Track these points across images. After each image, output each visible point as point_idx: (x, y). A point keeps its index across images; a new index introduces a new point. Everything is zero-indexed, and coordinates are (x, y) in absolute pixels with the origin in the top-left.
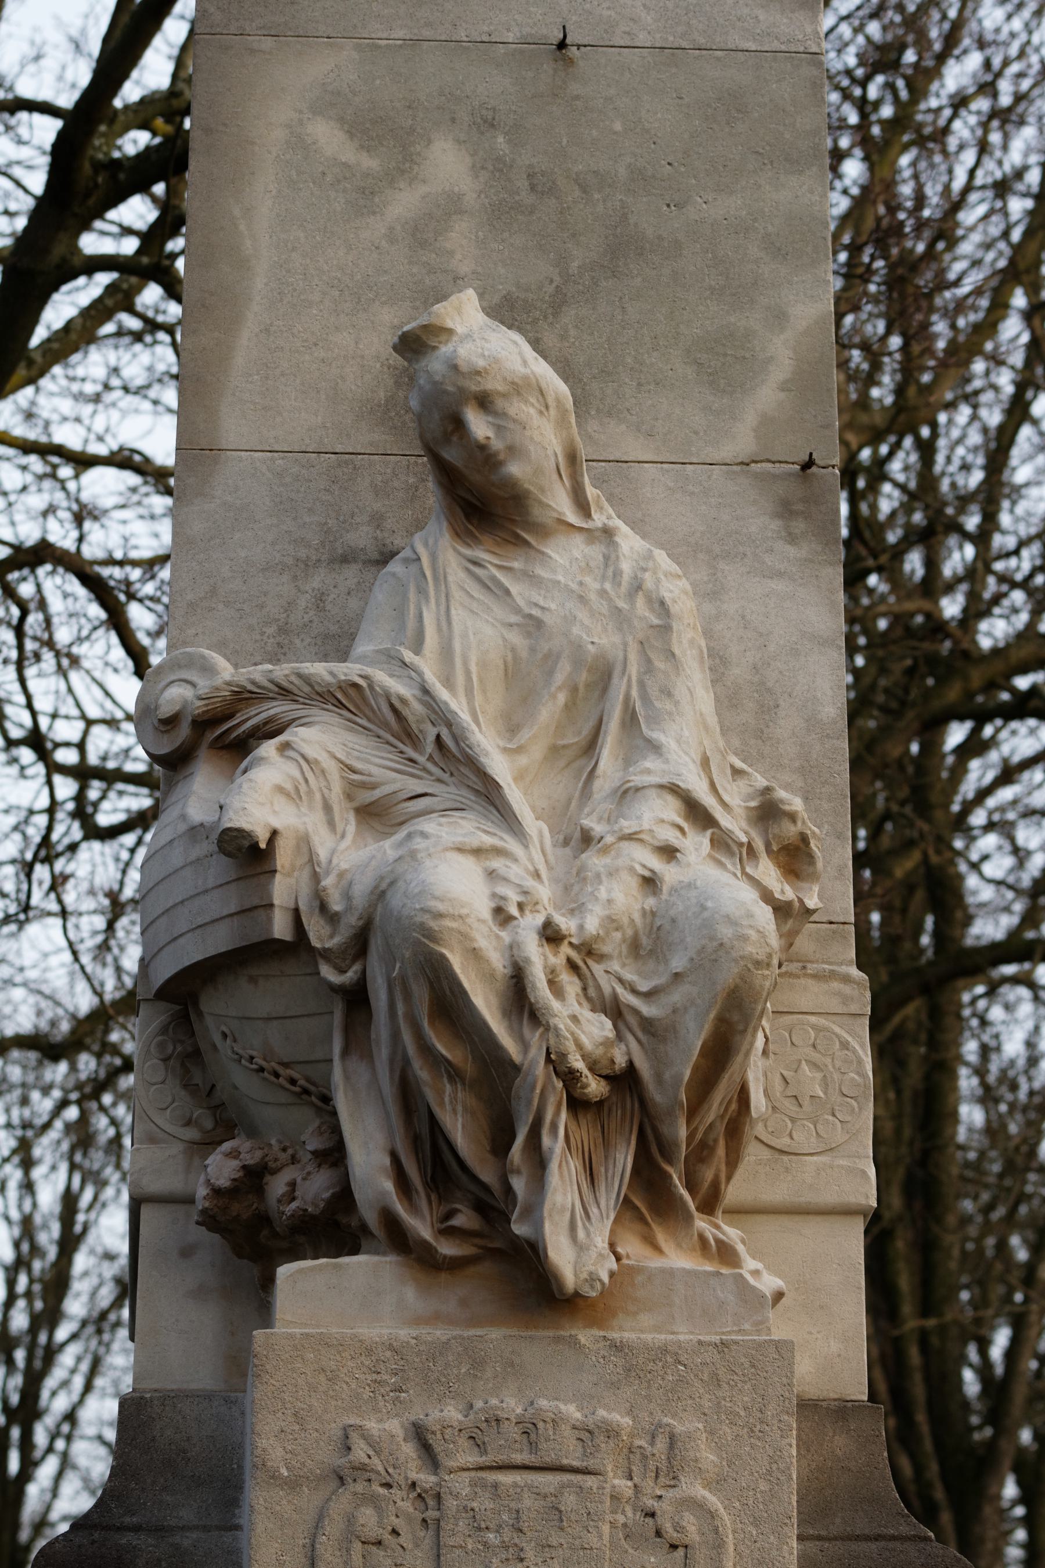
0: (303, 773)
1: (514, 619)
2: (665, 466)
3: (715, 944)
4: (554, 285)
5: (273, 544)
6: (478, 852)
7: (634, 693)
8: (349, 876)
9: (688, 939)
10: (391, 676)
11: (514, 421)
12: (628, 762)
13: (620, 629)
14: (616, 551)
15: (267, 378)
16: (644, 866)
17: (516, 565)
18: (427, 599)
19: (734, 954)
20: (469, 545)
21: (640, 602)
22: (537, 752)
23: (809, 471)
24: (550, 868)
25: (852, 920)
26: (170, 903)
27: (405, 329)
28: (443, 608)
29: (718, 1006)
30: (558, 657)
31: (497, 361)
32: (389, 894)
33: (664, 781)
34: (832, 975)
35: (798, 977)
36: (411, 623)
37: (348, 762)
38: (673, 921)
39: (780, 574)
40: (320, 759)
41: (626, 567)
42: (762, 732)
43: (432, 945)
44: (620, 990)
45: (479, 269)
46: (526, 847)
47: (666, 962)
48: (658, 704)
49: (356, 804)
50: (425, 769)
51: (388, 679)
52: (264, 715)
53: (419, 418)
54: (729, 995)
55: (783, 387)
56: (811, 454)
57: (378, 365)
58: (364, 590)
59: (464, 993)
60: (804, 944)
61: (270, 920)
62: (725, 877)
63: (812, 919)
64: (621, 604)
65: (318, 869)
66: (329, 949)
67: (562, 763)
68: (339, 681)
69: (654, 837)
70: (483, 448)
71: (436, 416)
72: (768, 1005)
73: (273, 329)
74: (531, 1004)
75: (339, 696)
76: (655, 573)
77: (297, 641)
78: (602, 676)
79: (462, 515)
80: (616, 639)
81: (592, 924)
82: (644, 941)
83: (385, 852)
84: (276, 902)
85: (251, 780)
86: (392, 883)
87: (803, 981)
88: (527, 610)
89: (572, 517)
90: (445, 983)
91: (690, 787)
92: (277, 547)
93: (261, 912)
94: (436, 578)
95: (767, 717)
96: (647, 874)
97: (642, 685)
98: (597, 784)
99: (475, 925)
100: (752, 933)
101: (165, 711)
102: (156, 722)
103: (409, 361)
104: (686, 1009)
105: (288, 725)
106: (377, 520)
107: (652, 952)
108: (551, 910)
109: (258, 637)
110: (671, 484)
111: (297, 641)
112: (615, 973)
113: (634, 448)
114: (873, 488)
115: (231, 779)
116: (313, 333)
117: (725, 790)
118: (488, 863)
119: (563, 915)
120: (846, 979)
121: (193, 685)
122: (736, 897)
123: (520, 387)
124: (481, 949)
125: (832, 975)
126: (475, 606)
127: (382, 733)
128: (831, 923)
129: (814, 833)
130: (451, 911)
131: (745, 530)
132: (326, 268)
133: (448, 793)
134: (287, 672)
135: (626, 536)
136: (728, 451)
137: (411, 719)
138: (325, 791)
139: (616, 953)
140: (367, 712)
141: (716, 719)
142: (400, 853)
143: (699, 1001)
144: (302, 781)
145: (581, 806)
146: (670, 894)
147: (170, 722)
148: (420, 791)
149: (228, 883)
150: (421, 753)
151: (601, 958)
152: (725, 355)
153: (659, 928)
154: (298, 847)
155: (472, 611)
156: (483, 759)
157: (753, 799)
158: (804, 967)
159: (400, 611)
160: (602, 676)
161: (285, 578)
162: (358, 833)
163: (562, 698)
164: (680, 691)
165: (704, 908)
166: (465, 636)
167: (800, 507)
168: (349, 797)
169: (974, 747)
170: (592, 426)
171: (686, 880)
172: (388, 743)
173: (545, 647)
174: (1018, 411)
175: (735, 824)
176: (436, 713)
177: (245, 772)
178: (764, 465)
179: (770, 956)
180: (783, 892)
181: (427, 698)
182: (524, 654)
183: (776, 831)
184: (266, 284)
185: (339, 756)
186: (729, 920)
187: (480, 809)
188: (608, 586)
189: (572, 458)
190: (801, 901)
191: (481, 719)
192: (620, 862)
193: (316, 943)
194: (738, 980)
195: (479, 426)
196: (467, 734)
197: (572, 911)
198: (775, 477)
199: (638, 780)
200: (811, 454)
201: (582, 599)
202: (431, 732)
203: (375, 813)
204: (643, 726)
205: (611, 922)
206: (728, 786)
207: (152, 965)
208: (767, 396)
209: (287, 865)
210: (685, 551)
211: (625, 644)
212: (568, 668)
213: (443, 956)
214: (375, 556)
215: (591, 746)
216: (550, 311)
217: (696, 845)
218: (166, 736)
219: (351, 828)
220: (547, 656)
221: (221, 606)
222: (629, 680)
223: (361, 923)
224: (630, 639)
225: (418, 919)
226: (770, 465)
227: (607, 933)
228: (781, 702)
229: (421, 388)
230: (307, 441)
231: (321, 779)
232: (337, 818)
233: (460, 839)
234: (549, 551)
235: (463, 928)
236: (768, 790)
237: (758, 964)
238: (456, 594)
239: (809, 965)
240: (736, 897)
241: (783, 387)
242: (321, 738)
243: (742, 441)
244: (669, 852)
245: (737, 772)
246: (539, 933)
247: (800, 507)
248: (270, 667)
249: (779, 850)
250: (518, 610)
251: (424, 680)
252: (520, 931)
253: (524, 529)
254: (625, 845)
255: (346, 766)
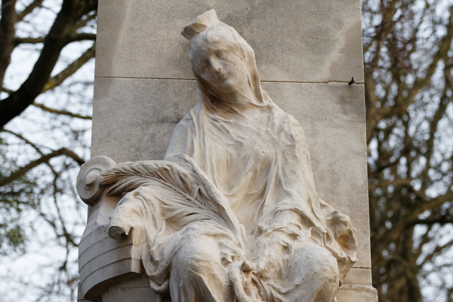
0: (144, 205)
1: (231, 142)
2: (293, 83)
3: (313, 272)
4: (248, 11)
5: (134, 115)
6: (215, 236)
7: (280, 172)
8: (162, 246)
9: (302, 271)
10: (181, 166)
11: (231, 62)
12: (277, 201)
13: (274, 147)
14: (272, 115)
15: (131, 48)
16: (284, 242)
17: (232, 121)
18: (195, 135)
19: (321, 277)
20: (212, 113)
21: (283, 137)
22: (240, 196)
23: (352, 85)
24: (245, 243)
25: (371, 267)
26: (90, 259)
27: (186, 25)
28: (202, 138)
29: (314, 298)
30: (249, 158)
31: (223, 38)
32: (178, 253)
33: (292, 207)
34: (362, 289)
35: (348, 290)
36: (189, 145)
37: (163, 200)
38: (296, 264)
39: (340, 127)
40: (151, 199)
41: (277, 122)
42: (333, 190)
43: (196, 273)
44: (274, 292)
45: (218, 5)
46: (235, 234)
47: (293, 281)
48: (290, 177)
49: (166, 218)
50: (194, 203)
51: (179, 166)
52: (128, 182)
53: (192, 61)
54: (319, 293)
55: (342, 51)
56: (353, 78)
57: (177, 43)
58: (170, 133)
59: (209, 292)
60: (351, 276)
61: (130, 264)
62: (317, 246)
63: (353, 266)
64: (275, 136)
65: (150, 244)
66: (154, 276)
67: (251, 201)
68: (159, 168)
69: (288, 230)
70: (218, 73)
71: (199, 60)
72: (335, 298)
73: (134, 29)
74: (237, 297)
75: (159, 174)
76: (288, 124)
77: (144, 154)
78: (267, 166)
79: (209, 101)
80: (273, 150)
81: (262, 265)
82: (284, 272)
83: (177, 236)
84: (133, 257)
85: (122, 207)
86: (180, 249)
87: (350, 291)
88: (236, 139)
89: (255, 102)
90: (201, 289)
91: (303, 210)
92: (135, 116)
93: (127, 261)
94: (199, 126)
95: (335, 184)
96: (285, 245)
97: (283, 169)
98: (265, 209)
99: (214, 265)
100: (328, 268)
101: (89, 181)
102: (85, 186)
103: (188, 39)
104: (301, 299)
105: (138, 186)
106: (176, 105)
107: (287, 277)
108: (245, 259)
109: (127, 153)
110: (296, 91)
111: (144, 154)
112: (272, 285)
113: (280, 76)
114: (387, 138)
115: (115, 208)
116: (150, 30)
117: (318, 212)
118: (219, 240)
119: (250, 261)
120: (368, 291)
121: (100, 170)
122: (323, 255)
123: (232, 49)
124: (216, 274)
125: (362, 289)
126: (215, 137)
127: (176, 189)
128: (362, 268)
129: (354, 230)
130: (203, 259)
131: (326, 109)
132: (156, 4)
133: (203, 213)
134: (138, 164)
135: (277, 109)
136: (319, 77)
137: (188, 183)
138: (153, 212)
139: (272, 277)
140: (170, 180)
141: (314, 183)
142: (183, 236)
143: (306, 296)
144: (143, 208)
145: (258, 219)
146: (295, 253)
147: (91, 186)
148: (192, 212)
149: (113, 250)
150: (192, 197)
151: (266, 279)
152: (318, 39)
153: (290, 267)
154: (142, 234)
155: (214, 140)
156: (217, 198)
157: (329, 216)
158: (351, 286)
159: (184, 140)
160: (267, 166)
161: (139, 128)
162: (167, 229)
163: (250, 174)
164: (299, 172)
165: (308, 258)
166: (211, 150)
167: (348, 99)
168: (163, 215)
169: (425, 239)
170: (264, 67)
171: (301, 247)
172: (179, 193)
173: (243, 154)
174: (441, 112)
175: (322, 225)
176: (198, 180)
177: (121, 204)
178: (334, 83)
179: (335, 277)
180: (341, 254)
181: (195, 174)
182: (235, 157)
183: (339, 229)
184: (131, 11)
185: (159, 198)
186: (319, 263)
187: (216, 219)
188: (269, 129)
189: (255, 78)
190: (349, 258)
191: (217, 183)
192: (274, 240)
193: (149, 273)
194: (322, 287)
195: (216, 64)
196: (211, 188)
197: (254, 260)
198: (338, 87)
199: (281, 207)
200: (353, 78)
201: (259, 135)
202: (197, 188)
203: (174, 221)
204: (283, 185)
205: (270, 265)
206: (319, 211)
207: (83, 285)
208: (335, 55)
209: (137, 242)
210: (302, 117)
211: (276, 153)
212: (253, 162)
213: (200, 277)
214: (175, 120)
215: (262, 194)
216: (247, 21)
217: (305, 234)
218: (89, 192)
219: (164, 227)
220: (244, 158)
221: (112, 140)
222: (278, 167)
223: (167, 265)
224: (278, 150)
225: (190, 262)
226: (336, 83)
227: (269, 269)
228: (341, 178)
229: (193, 49)
230: (148, 74)
231: (151, 207)
232: (158, 223)
233: (208, 230)
234: (245, 115)
235: (208, 266)
236: (335, 212)
237: (330, 281)
238: (207, 133)
239: (353, 285)
240: (323, 255)
241: (342, 51)
242: (152, 191)
243: (324, 73)
244: (294, 236)
245: (322, 206)
246: (240, 268)
247: (348, 99)
248: (131, 162)
249: (340, 237)
250: (232, 139)
251: (194, 167)
252: (232, 267)
253: (234, 106)
254: (276, 233)
255: (162, 202)
